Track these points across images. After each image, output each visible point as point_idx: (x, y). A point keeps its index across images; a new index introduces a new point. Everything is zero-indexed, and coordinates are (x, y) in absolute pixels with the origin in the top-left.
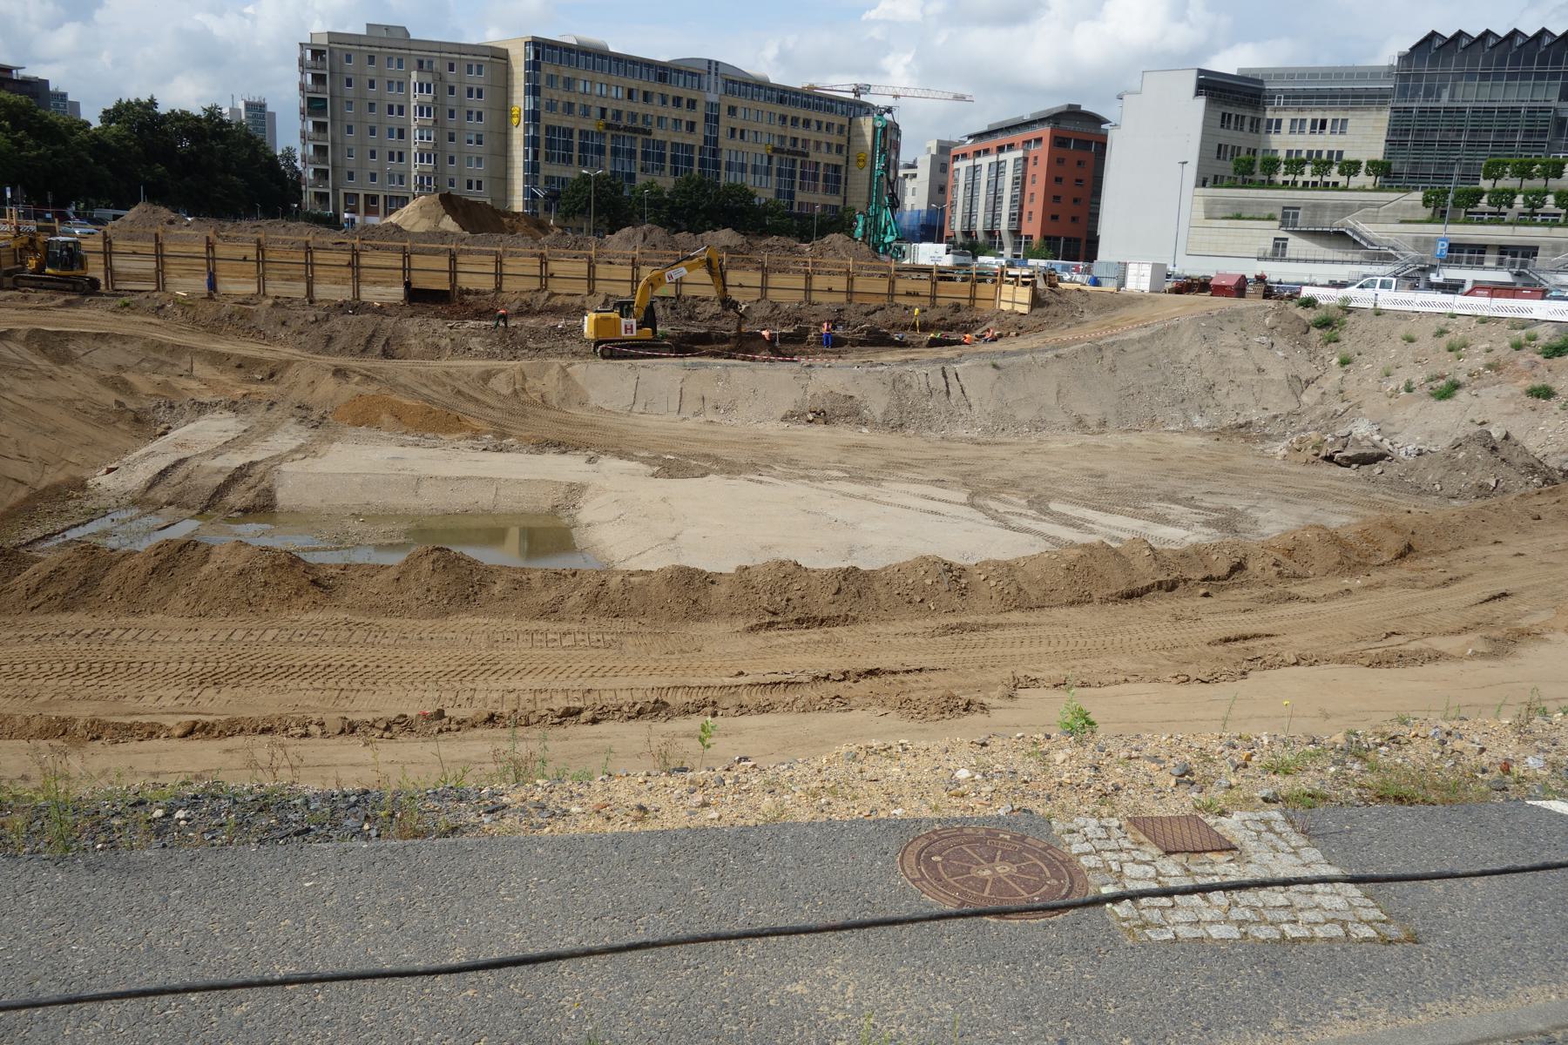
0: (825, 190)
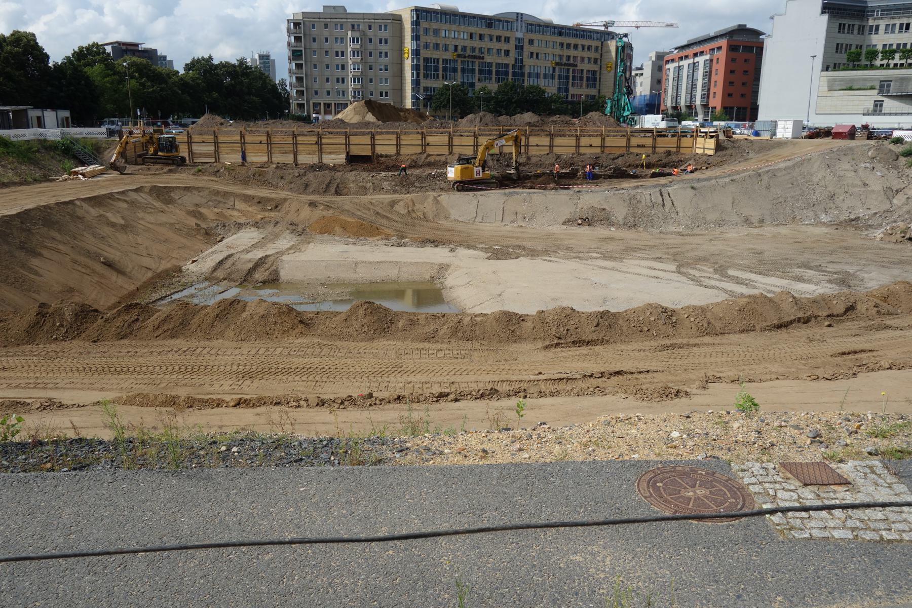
0: (587, 86)
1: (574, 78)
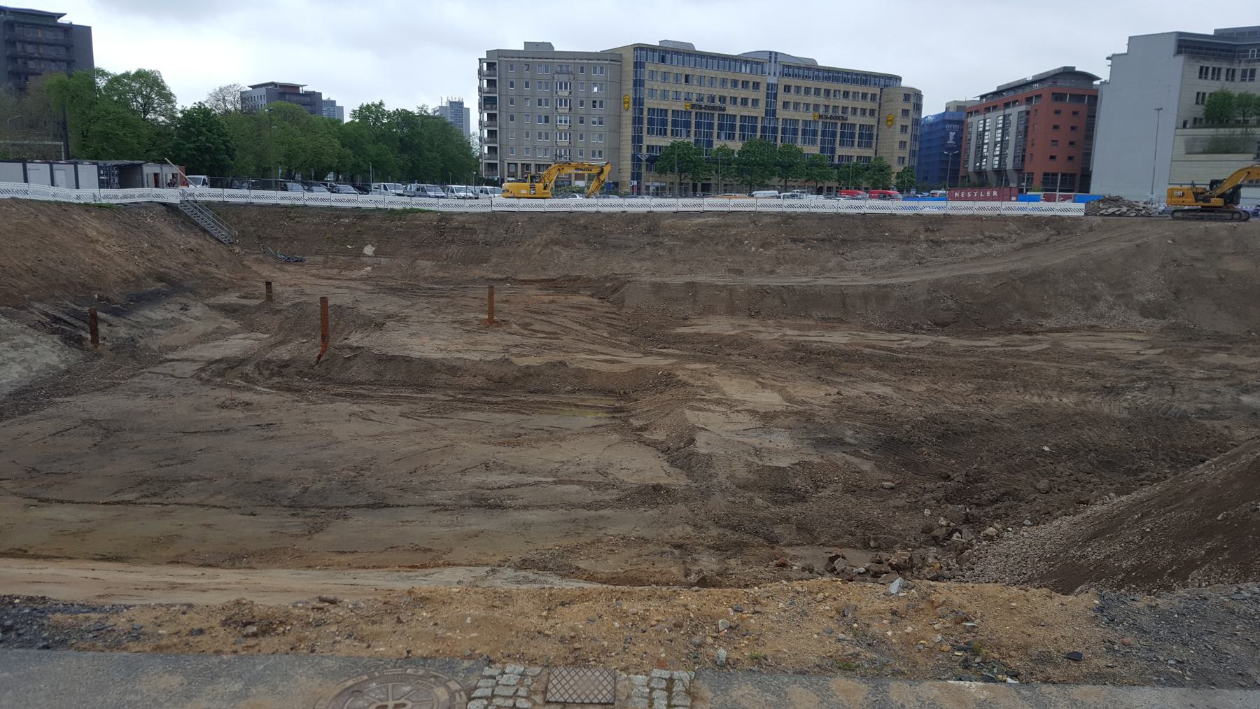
1: (698, 125)
